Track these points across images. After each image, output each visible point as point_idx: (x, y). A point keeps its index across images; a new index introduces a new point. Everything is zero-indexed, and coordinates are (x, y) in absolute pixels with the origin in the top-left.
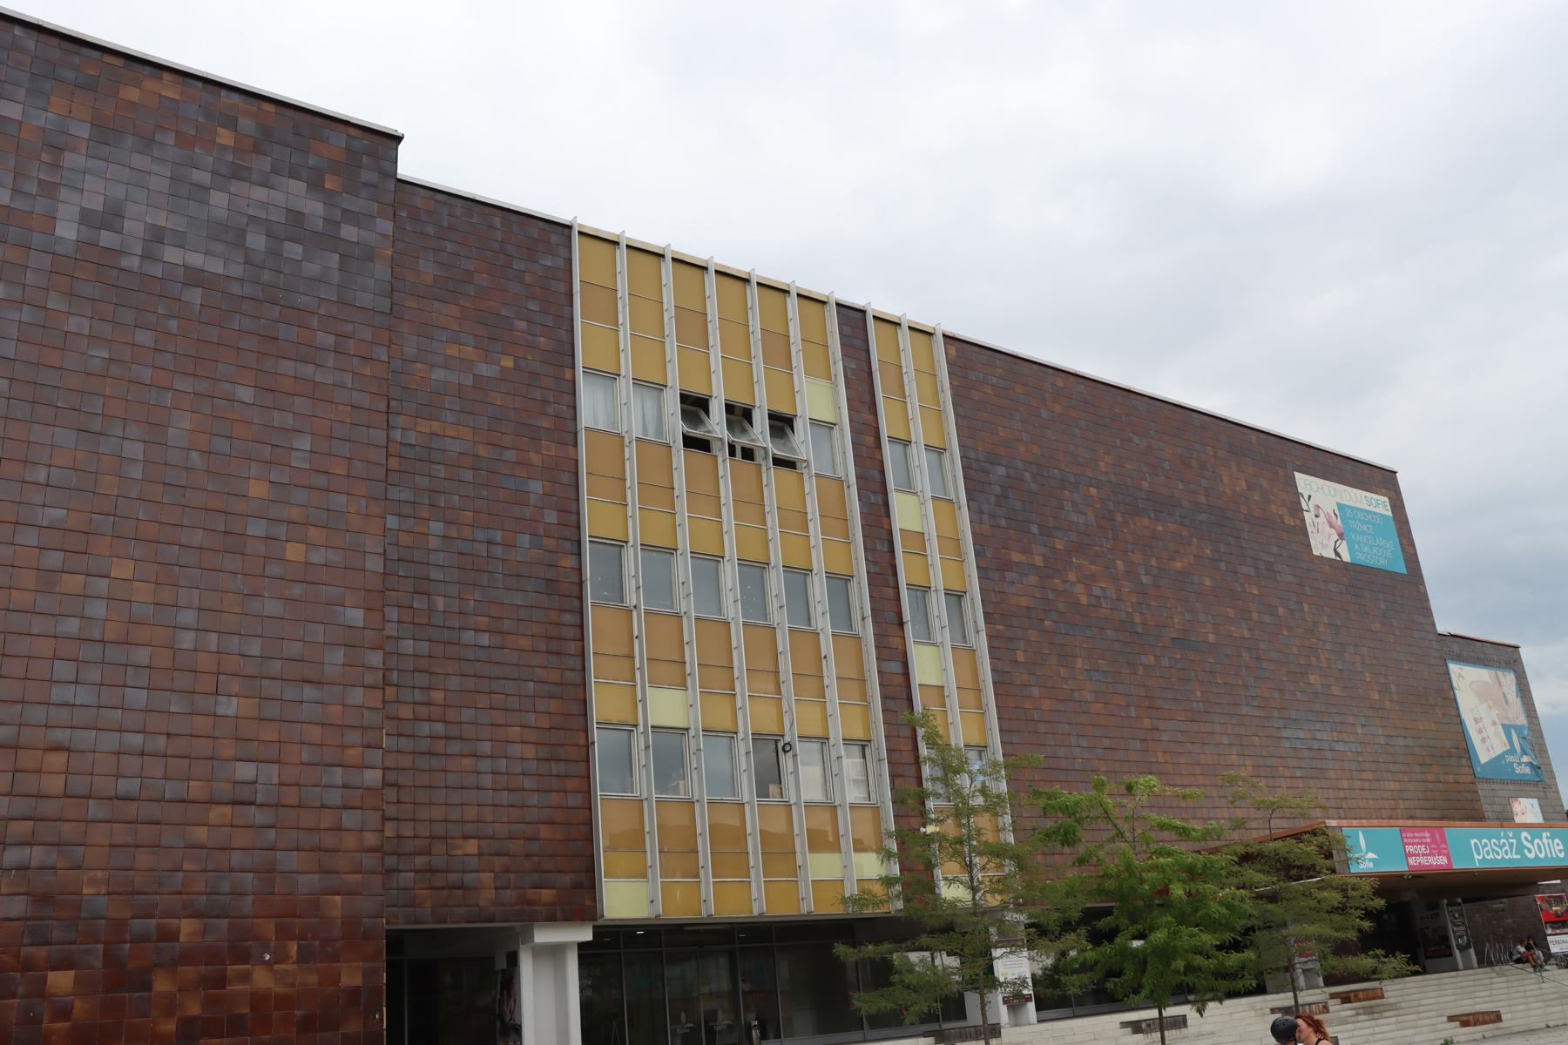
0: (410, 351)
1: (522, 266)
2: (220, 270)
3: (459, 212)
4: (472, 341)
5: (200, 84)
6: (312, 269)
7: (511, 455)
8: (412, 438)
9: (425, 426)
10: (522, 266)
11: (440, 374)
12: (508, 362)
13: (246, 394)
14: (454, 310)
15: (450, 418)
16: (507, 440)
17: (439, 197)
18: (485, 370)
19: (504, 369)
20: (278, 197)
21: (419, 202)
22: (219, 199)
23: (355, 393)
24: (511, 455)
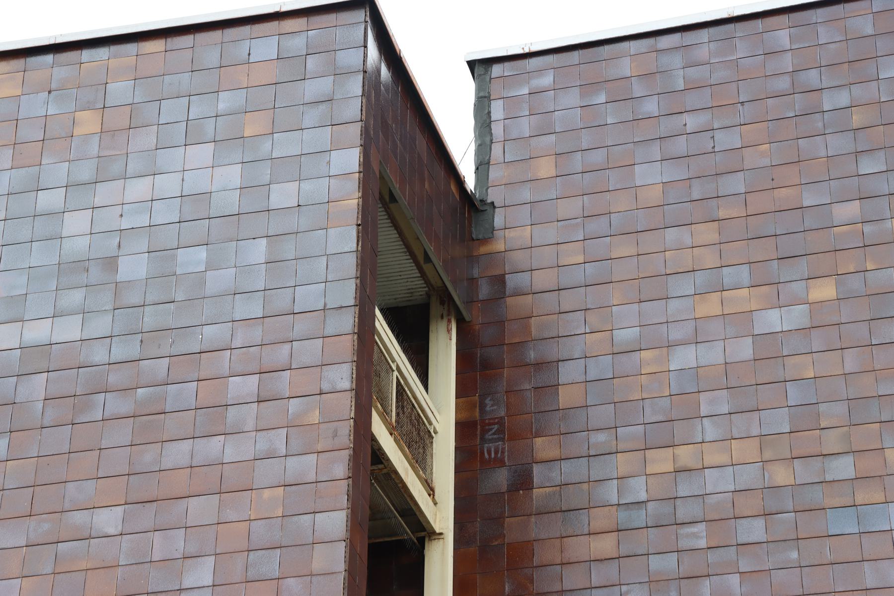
0: (626, 335)
1: (843, 98)
2: (75, 334)
3: (703, 53)
4: (744, 274)
5: (49, 58)
6: (221, 279)
7: (843, 468)
8: (639, 490)
9: (661, 461)
10: (843, 98)
11: (685, 358)
12: (825, 290)
13: (108, 520)
14: (707, 233)
15: (711, 430)
16: (832, 441)
17: (665, 42)
18: (773, 320)
19: (815, 306)
20: (168, 184)
21: (626, 67)
22: (76, 223)
23: (292, 462)
24: (843, 468)
